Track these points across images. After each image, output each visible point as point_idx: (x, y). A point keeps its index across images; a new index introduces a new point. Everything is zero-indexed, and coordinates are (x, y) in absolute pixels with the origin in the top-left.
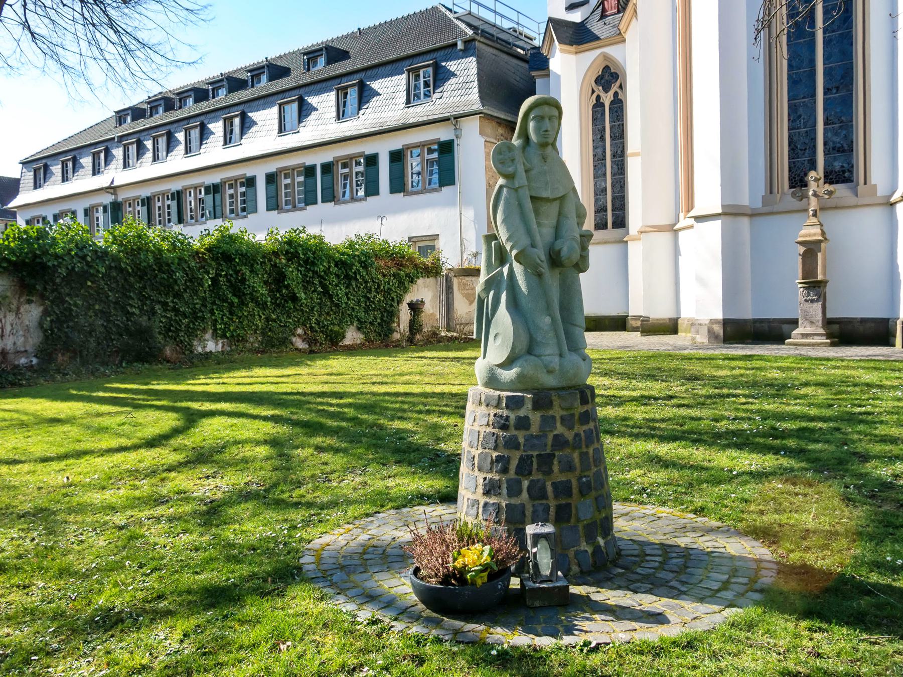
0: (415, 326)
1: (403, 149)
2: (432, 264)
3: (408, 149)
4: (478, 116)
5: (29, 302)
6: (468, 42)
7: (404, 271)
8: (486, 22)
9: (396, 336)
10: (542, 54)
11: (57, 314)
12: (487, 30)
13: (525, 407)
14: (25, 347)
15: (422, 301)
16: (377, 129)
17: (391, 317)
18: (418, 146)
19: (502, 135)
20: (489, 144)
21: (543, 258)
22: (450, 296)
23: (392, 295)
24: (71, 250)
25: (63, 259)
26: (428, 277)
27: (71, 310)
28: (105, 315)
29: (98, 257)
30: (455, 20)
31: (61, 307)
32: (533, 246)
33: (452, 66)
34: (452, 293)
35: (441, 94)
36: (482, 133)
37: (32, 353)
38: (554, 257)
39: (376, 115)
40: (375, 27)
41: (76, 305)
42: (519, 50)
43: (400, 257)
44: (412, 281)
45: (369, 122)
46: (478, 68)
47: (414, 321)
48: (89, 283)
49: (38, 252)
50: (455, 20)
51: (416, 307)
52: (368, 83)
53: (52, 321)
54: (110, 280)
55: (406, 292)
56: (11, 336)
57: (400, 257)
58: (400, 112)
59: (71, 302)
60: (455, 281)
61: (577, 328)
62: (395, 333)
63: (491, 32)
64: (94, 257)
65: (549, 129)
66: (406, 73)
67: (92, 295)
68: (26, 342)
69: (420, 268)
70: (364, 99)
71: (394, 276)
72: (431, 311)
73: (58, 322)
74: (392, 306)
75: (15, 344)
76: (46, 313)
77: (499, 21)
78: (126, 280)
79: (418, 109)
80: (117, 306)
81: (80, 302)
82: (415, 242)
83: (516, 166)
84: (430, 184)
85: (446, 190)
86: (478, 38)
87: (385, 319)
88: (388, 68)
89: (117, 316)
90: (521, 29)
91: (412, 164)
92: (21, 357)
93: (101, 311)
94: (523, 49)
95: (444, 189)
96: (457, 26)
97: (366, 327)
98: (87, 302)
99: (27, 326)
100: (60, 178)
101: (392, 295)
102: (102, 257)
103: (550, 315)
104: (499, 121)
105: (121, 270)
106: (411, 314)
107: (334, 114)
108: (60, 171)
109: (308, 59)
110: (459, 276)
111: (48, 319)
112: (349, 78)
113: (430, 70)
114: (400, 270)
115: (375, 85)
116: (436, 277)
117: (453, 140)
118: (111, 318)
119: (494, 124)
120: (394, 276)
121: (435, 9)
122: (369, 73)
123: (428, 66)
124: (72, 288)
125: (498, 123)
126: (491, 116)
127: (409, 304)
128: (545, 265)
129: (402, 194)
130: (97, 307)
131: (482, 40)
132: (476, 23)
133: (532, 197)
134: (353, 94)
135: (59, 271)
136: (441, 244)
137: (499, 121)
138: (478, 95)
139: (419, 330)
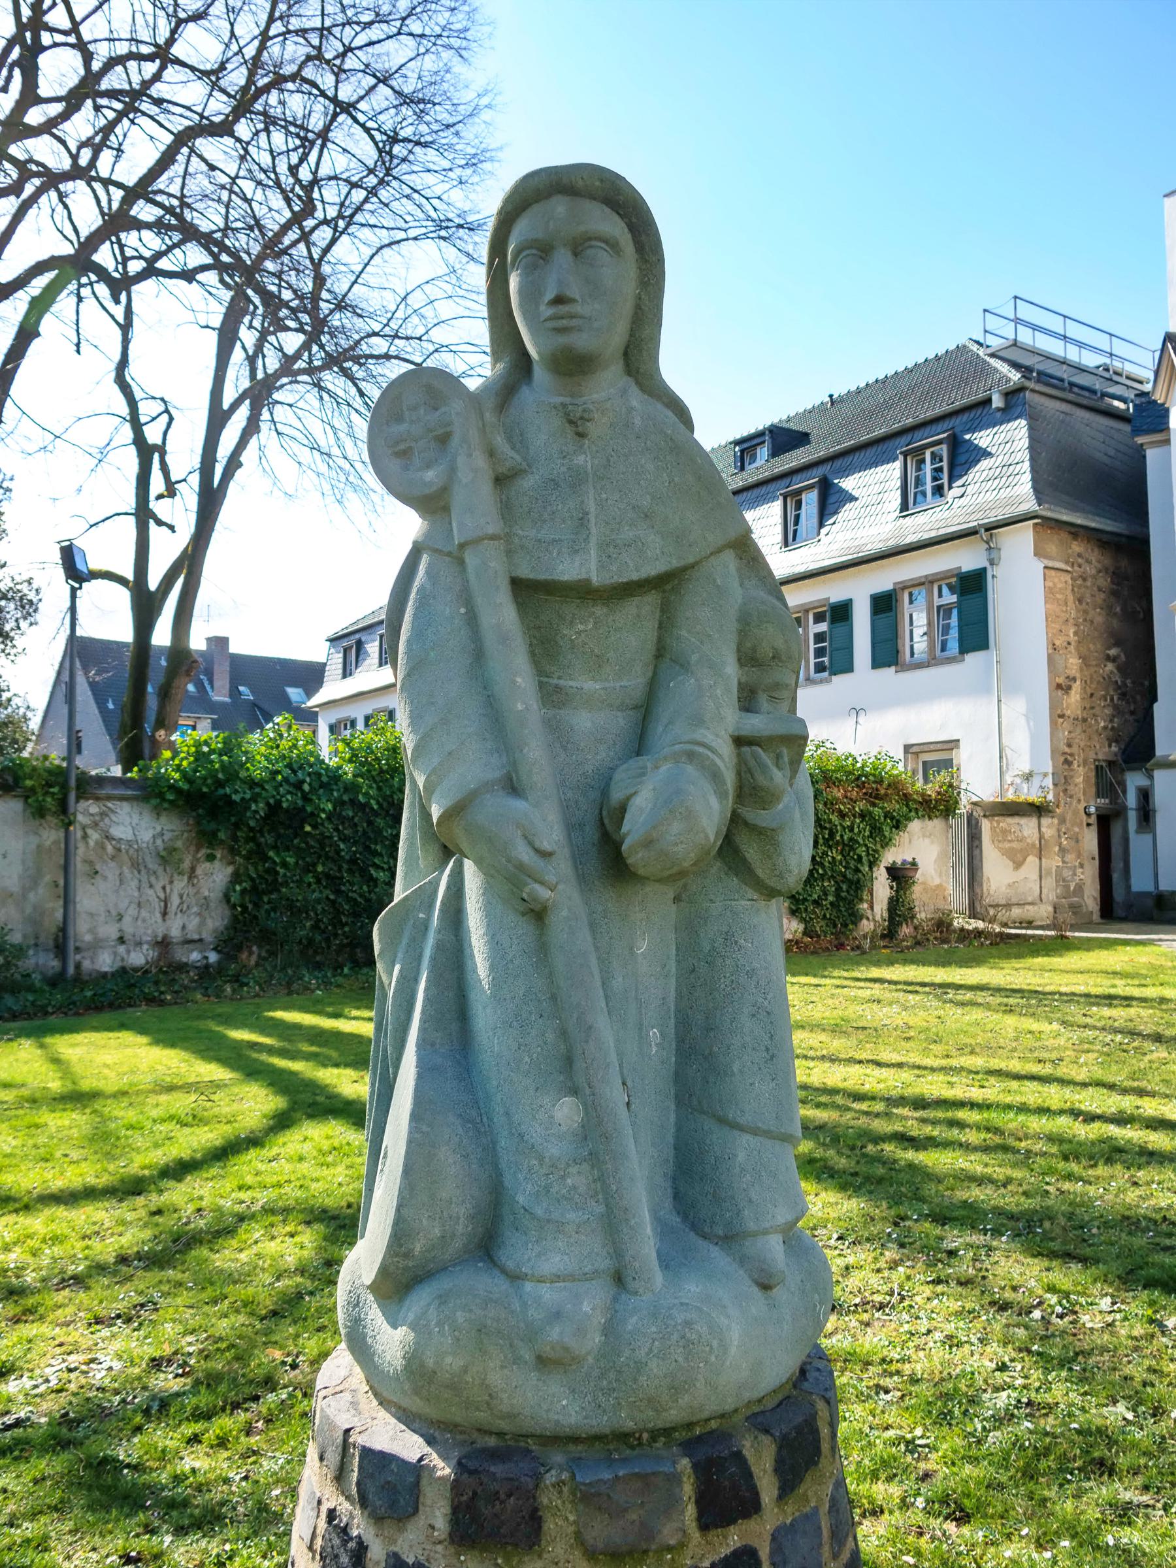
0: (898, 910)
1: (895, 590)
2: (939, 793)
3: (903, 589)
4: (1031, 522)
5: (211, 858)
6: (1009, 395)
7: (882, 808)
8: (1048, 357)
9: (866, 926)
10: (1155, 402)
11: (252, 879)
12: (1050, 371)
13: (421, 1521)
14: (200, 934)
15: (914, 864)
16: (850, 557)
17: (856, 891)
18: (923, 584)
19: (1079, 555)
20: (1053, 573)
21: (552, 835)
22: (976, 852)
23: (858, 851)
24: (278, 772)
25: (264, 789)
26: (930, 818)
27: (277, 873)
28: (333, 881)
29: (322, 785)
30: (988, 359)
31: (260, 868)
32: (512, 786)
33: (983, 438)
34: (980, 847)
35: (963, 489)
36: (1038, 553)
37: (211, 943)
38: (609, 827)
39: (849, 535)
40: (859, 391)
41: (284, 864)
42: (1116, 403)
43: (875, 782)
44: (897, 826)
45: (834, 547)
46: (1030, 437)
47: (897, 900)
48: (308, 828)
49: (220, 776)
50: (988, 359)
51: (900, 874)
52: (836, 481)
53: (243, 891)
54: (343, 823)
55: (887, 844)
56: (179, 915)
57: (875, 782)
58: (890, 526)
59: (277, 860)
60: (986, 825)
61: (746, 1139)
62: (865, 922)
63: (1058, 374)
64: (315, 784)
65: (573, 292)
66: (901, 457)
67: (313, 847)
68: (202, 923)
69: (914, 800)
70: (830, 508)
71: (862, 816)
72: (937, 881)
73: (255, 892)
74: (857, 870)
75: (184, 927)
76: (236, 878)
77: (1073, 354)
78: (370, 823)
79: (921, 519)
80: (354, 868)
81: (291, 860)
82: (917, 754)
83: (452, 470)
84: (943, 649)
85: (973, 659)
86: (1031, 385)
87: (843, 894)
88: (871, 452)
89: (352, 884)
90: (1117, 364)
91: (911, 616)
92: (192, 951)
93: (327, 876)
94: (1124, 400)
95: (970, 658)
96: (996, 370)
97: (806, 910)
98: (303, 859)
99: (205, 898)
100: (377, 661)
101: (858, 851)
102: (328, 784)
103: (575, 1092)
104: (1073, 530)
105: (363, 807)
106: (892, 888)
107: (779, 537)
108: (377, 649)
109: (742, 451)
110: (994, 815)
111: (238, 888)
112: (804, 475)
113: (944, 450)
114: (874, 805)
115: (848, 484)
116: (946, 817)
117: (985, 569)
118: (343, 888)
119: (1064, 535)
120: (862, 816)
121: (961, 349)
122: (838, 463)
123: (939, 442)
124: (279, 836)
125: (1070, 533)
126: (1057, 521)
127: (888, 869)
128: (561, 868)
129: (893, 669)
130: (320, 869)
131: (1039, 387)
132: (1028, 361)
133: (524, 590)
134: (811, 500)
135: (254, 807)
136: (962, 756)
137: (1073, 530)
138: (1030, 484)
139: (910, 916)
